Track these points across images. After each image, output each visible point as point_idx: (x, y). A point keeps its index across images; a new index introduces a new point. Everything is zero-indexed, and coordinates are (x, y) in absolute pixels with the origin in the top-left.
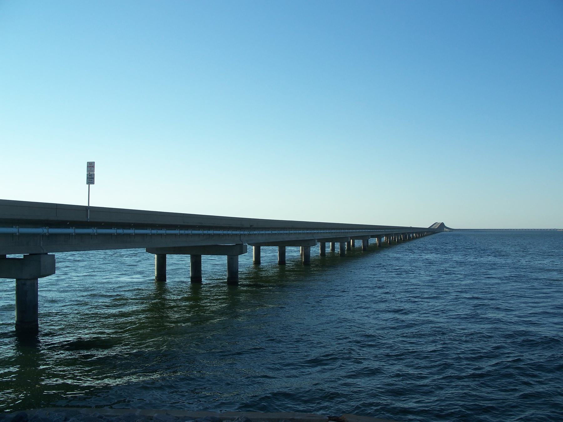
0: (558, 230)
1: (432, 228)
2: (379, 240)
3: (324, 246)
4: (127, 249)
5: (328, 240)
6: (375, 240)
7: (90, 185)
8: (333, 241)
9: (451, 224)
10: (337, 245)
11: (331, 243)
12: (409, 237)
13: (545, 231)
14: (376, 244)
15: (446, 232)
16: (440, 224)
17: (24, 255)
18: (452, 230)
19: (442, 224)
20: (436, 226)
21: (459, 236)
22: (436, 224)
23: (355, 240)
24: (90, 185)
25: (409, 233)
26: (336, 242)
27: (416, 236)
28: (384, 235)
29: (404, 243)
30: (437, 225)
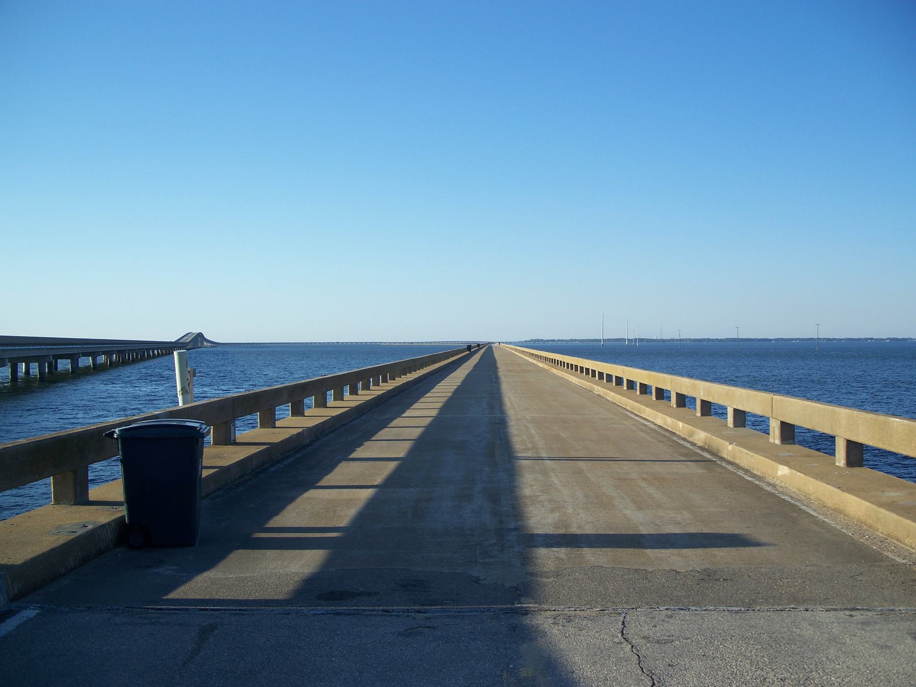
0: (391, 344)
1: (181, 341)
2: (94, 360)
3: (29, 366)
4: (694, 426)
5: (22, 359)
6: (90, 360)
7: (204, 464)
8: (28, 360)
9: (216, 334)
10: (156, 351)
11: (24, 363)
12: (149, 355)
13: (373, 345)
14: (90, 366)
15: (205, 349)
16: (195, 334)
17: (373, 386)
18: (215, 344)
19: (200, 335)
20: (187, 339)
21: (224, 353)
22: (190, 335)
23: (58, 360)
24: (204, 464)
25: (148, 350)
26: (32, 362)
27: (162, 352)
28: (81, 354)
29: (123, 366)
30: (190, 336)
